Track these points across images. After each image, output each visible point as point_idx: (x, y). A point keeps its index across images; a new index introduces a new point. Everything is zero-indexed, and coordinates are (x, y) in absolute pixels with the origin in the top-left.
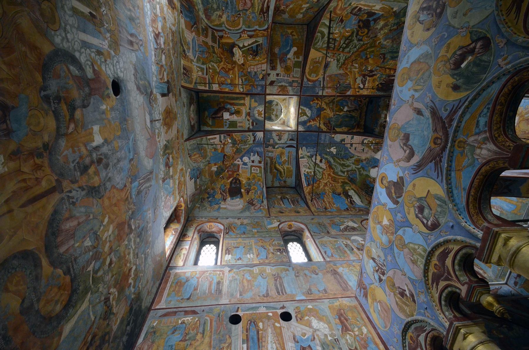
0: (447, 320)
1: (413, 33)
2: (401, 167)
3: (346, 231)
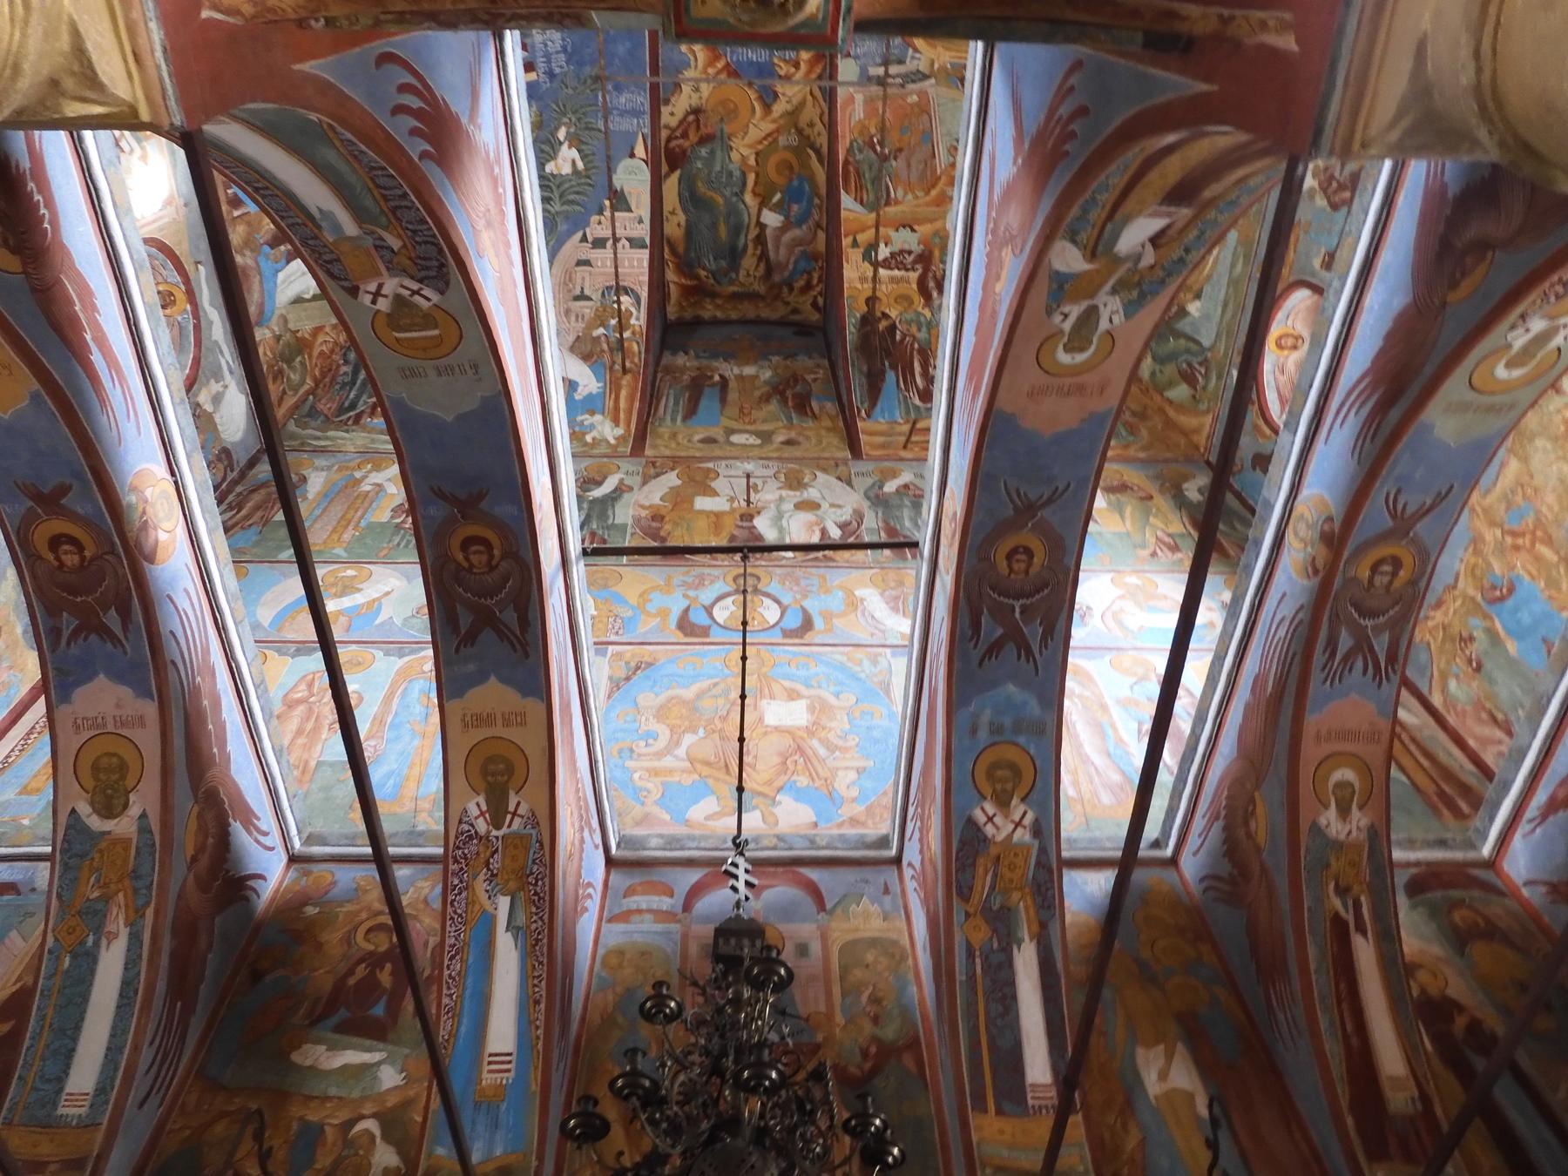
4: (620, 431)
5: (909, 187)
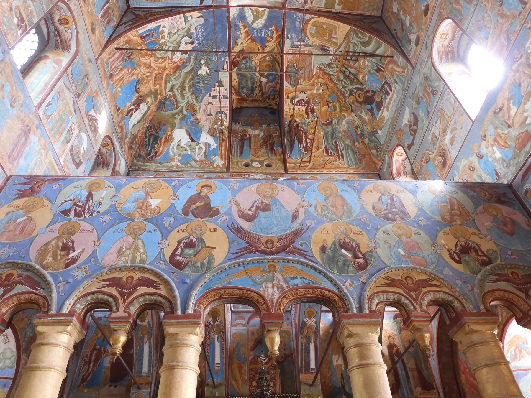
0: (69, 309)
1: (371, 191)
2: (230, 208)
3: (89, 121)
4: (223, 162)
5: (304, 79)
